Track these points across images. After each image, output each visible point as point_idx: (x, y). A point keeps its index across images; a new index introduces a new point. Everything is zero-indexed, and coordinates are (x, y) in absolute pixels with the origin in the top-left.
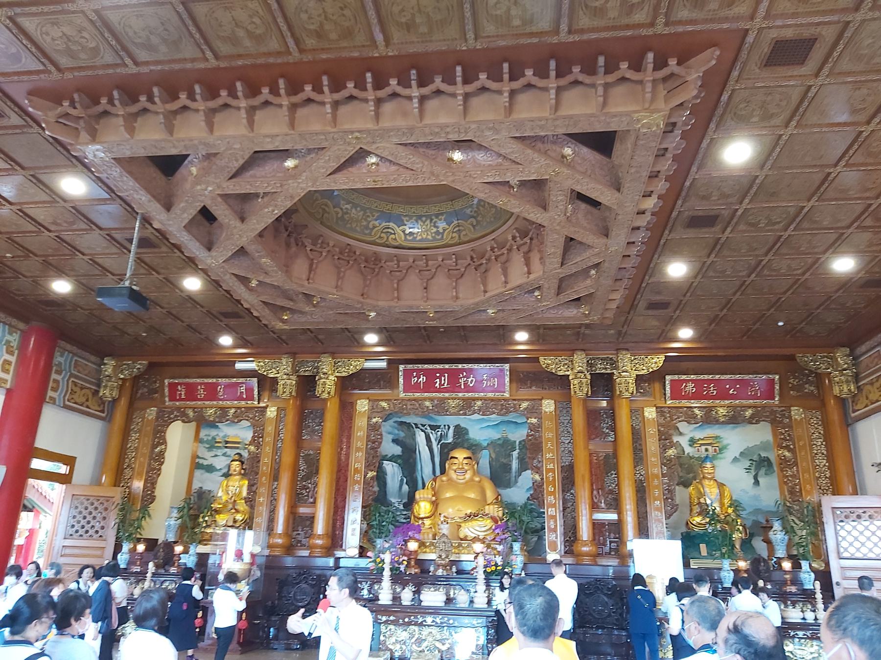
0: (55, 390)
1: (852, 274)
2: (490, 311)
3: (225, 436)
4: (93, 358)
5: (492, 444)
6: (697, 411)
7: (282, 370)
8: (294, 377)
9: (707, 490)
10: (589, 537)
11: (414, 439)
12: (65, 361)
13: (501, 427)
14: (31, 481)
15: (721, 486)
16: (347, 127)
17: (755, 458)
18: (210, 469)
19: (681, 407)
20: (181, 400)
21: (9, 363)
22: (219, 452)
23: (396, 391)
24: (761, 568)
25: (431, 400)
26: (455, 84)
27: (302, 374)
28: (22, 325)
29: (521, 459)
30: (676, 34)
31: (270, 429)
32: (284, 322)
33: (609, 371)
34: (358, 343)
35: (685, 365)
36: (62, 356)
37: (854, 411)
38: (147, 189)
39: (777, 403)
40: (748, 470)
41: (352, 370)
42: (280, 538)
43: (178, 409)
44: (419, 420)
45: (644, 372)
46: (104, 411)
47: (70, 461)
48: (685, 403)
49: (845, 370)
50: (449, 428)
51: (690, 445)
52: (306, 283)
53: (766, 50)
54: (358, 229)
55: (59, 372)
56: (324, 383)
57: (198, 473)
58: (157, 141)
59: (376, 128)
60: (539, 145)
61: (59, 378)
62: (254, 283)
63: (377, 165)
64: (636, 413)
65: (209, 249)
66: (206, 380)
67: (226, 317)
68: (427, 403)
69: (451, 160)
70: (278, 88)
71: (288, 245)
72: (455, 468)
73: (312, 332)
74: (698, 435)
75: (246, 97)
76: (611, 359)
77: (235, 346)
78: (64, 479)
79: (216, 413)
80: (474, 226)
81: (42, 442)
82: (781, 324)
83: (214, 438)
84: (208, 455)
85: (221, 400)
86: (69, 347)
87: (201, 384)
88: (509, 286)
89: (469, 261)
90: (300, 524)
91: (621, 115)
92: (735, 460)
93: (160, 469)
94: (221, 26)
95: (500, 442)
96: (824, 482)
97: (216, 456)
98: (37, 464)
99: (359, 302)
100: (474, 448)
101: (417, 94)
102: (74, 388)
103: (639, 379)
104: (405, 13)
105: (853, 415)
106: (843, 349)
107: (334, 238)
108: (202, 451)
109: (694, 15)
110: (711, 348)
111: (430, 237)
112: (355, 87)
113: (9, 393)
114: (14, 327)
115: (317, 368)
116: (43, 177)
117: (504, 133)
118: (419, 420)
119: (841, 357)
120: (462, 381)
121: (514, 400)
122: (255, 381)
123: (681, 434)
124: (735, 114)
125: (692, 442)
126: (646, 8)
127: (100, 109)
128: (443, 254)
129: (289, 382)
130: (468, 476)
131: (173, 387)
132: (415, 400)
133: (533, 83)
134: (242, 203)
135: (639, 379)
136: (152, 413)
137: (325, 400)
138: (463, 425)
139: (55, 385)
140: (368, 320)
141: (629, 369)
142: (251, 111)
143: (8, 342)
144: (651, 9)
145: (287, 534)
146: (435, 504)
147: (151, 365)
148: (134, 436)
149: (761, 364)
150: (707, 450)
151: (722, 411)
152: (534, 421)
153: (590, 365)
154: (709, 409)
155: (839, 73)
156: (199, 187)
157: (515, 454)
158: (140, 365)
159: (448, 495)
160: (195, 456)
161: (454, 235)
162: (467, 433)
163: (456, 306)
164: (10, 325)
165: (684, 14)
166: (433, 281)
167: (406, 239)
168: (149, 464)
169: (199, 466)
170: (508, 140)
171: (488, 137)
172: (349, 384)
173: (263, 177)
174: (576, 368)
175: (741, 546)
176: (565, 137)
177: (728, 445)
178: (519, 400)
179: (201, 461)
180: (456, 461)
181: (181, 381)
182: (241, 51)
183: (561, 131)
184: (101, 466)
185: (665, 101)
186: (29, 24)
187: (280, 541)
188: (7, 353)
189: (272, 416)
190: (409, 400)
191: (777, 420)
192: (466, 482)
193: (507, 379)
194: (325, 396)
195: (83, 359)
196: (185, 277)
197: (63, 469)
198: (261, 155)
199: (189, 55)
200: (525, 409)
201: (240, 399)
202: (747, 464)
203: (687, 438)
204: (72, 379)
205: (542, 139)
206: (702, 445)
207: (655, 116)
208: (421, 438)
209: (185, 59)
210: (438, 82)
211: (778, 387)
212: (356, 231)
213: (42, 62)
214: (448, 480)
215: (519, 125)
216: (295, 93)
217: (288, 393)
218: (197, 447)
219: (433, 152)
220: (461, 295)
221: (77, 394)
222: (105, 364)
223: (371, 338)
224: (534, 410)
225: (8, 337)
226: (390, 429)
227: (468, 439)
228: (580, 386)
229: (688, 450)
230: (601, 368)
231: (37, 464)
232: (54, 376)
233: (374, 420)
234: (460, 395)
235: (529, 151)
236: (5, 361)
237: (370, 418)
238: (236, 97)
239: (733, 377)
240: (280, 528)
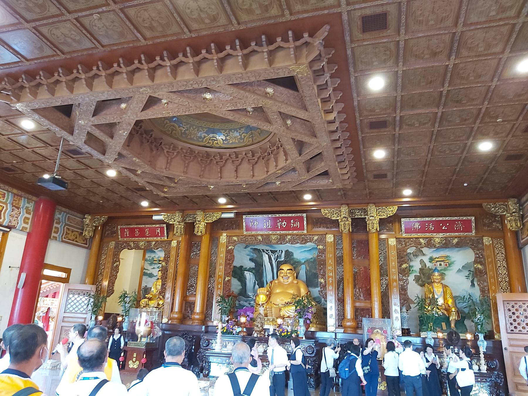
0: (56, 232)
1: (494, 152)
2: (278, 183)
3: (159, 257)
4: (79, 215)
5: (307, 261)
6: (421, 240)
7: (342, 214)
8: (183, 224)
9: (436, 289)
11: (262, 259)
12: (62, 217)
13: (312, 251)
14: (43, 281)
15: (445, 286)
16: (138, 84)
17: (472, 269)
18: (151, 275)
19: (412, 238)
20: (127, 237)
21: (28, 219)
22: (156, 266)
23: (242, 230)
24: (453, 338)
25: (262, 235)
26: (289, 41)
27: (188, 221)
28: (34, 198)
30: (299, 19)
31: (173, 253)
32: (164, 192)
33: (363, 217)
34: (299, 200)
35: (414, 212)
36: (60, 214)
37: (522, 239)
38: (56, 124)
39: (474, 234)
40: (467, 277)
41: (214, 219)
42: (177, 314)
43: (126, 242)
44: (265, 248)
45: (385, 217)
46: (87, 244)
47: (68, 271)
48: (414, 235)
49: (513, 213)
50: (282, 252)
51: (430, 262)
52: (164, 171)
53: (359, 23)
54: (195, 138)
55: (58, 223)
56: (199, 227)
57: (144, 278)
58: (47, 99)
59: (153, 84)
60: (249, 87)
61: (58, 226)
62: (139, 172)
63: (168, 103)
64: (383, 243)
65: (104, 154)
66: (139, 226)
67: (139, 191)
68: (260, 238)
69: (205, 99)
70: (211, 49)
71: (152, 150)
72: (282, 275)
73: (188, 198)
74: (435, 255)
75: (193, 56)
76: (364, 209)
77: (227, 204)
78: (65, 281)
79: (145, 244)
80: (259, 134)
81: (48, 260)
82: (465, 185)
83: (153, 258)
84: (150, 268)
85: (147, 237)
86: (64, 209)
87: (137, 228)
88: (278, 168)
89: (260, 154)
90: (187, 305)
91: (282, 68)
92: (459, 271)
93: (116, 276)
94: (58, 37)
95: (312, 260)
96: (504, 285)
97: (154, 268)
98: (47, 272)
99: (198, 180)
100: (295, 265)
101: (169, 64)
102: (68, 231)
103: (382, 222)
104: (145, 22)
105: (522, 241)
106: (513, 199)
107: (180, 144)
108: (147, 266)
109: (305, 8)
110: (425, 201)
111: (237, 141)
112: (231, 49)
113: (29, 235)
114: (30, 199)
115: (195, 218)
116: (11, 120)
117: (222, 83)
118: (265, 248)
119: (512, 205)
120: (279, 224)
121: (310, 235)
122: (165, 225)
123: (424, 255)
124: (361, 61)
125: (431, 260)
126: (275, 6)
127: (133, 67)
128: (245, 151)
129: (179, 226)
130: (290, 280)
131: (122, 230)
132: (252, 236)
133: (230, 53)
134: (110, 128)
135: (382, 222)
136: (112, 244)
137: (201, 237)
138: (290, 250)
139: (56, 230)
140: (210, 190)
141: (374, 216)
142: (271, 53)
143: (27, 208)
144: (278, 6)
145: (181, 311)
146: (269, 297)
147: (109, 218)
148: (103, 257)
149: (447, 210)
150: (440, 265)
151: (437, 240)
152: (321, 247)
153: (351, 213)
155: (471, 24)
156: (84, 122)
158: (104, 218)
159: (278, 291)
160: (143, 269)
161: (250, 139)
162: (293, 255)
163: (253, 180)
164: (28, 198)
165: (298, 7)
166: (240, 167)
167: (223, 143)
168: (111, 273)
169: (145, 274)
170: (227, 86)
171: (213, 85)
172: (215, 228)
173: (110, 114)
174: (342, 214)
175: (455, 325)
176: (265, 82)
177: (454, 261)
178: (313, 235)
179: (146, 271)
180: (283, 271)
181: (137, 226)
182: (74, 49)
183: (262, 78)
184: (86, 273)
185: (306, 59)
186: (45, 30)
187: (176, 316)
188: (26, 213)
189: (174, 246)
190: (249, 236)
191: (476, 245)
192: (289, 284)
193: (305, 223)
194: (200, 234)
195: (73, 215)
197: (63, 275)
198: (108, 102)
199: (223, 25)
200: (316, 240)
201: (157, 236)
202: (467, 273)
203: (428, 257)
204: (66, 227)
205: (251, 84)
206: (437, 261)
207: (302, 67)
208: (266, 258)
209: (49, 56)
210: (181, 57)
211: (474, 225)
212: (194, 140)
213: (54, 50)
215: (229, 77)
216: (246, 48)
217: (179, 232)
218: (144, 263)
219: (194, 95)
220: (256, 174)
221: (70, 235)
222: (85, 218)
223: (222, 200)
224: (322, 240)
225: (27, 205)
226: (248, 253)
227: (293, 259)
228: (346, 226)
229: (429, 265)
230: (358, 215)
231: (47, 272)
232: (55, 225)
233: (230, 247)
234: (278, 232)
235: (242, 92)
236: (25, 217)
237: (227, 247)
238: (235, 49)
239: (444, 219)
240: (176, 308)
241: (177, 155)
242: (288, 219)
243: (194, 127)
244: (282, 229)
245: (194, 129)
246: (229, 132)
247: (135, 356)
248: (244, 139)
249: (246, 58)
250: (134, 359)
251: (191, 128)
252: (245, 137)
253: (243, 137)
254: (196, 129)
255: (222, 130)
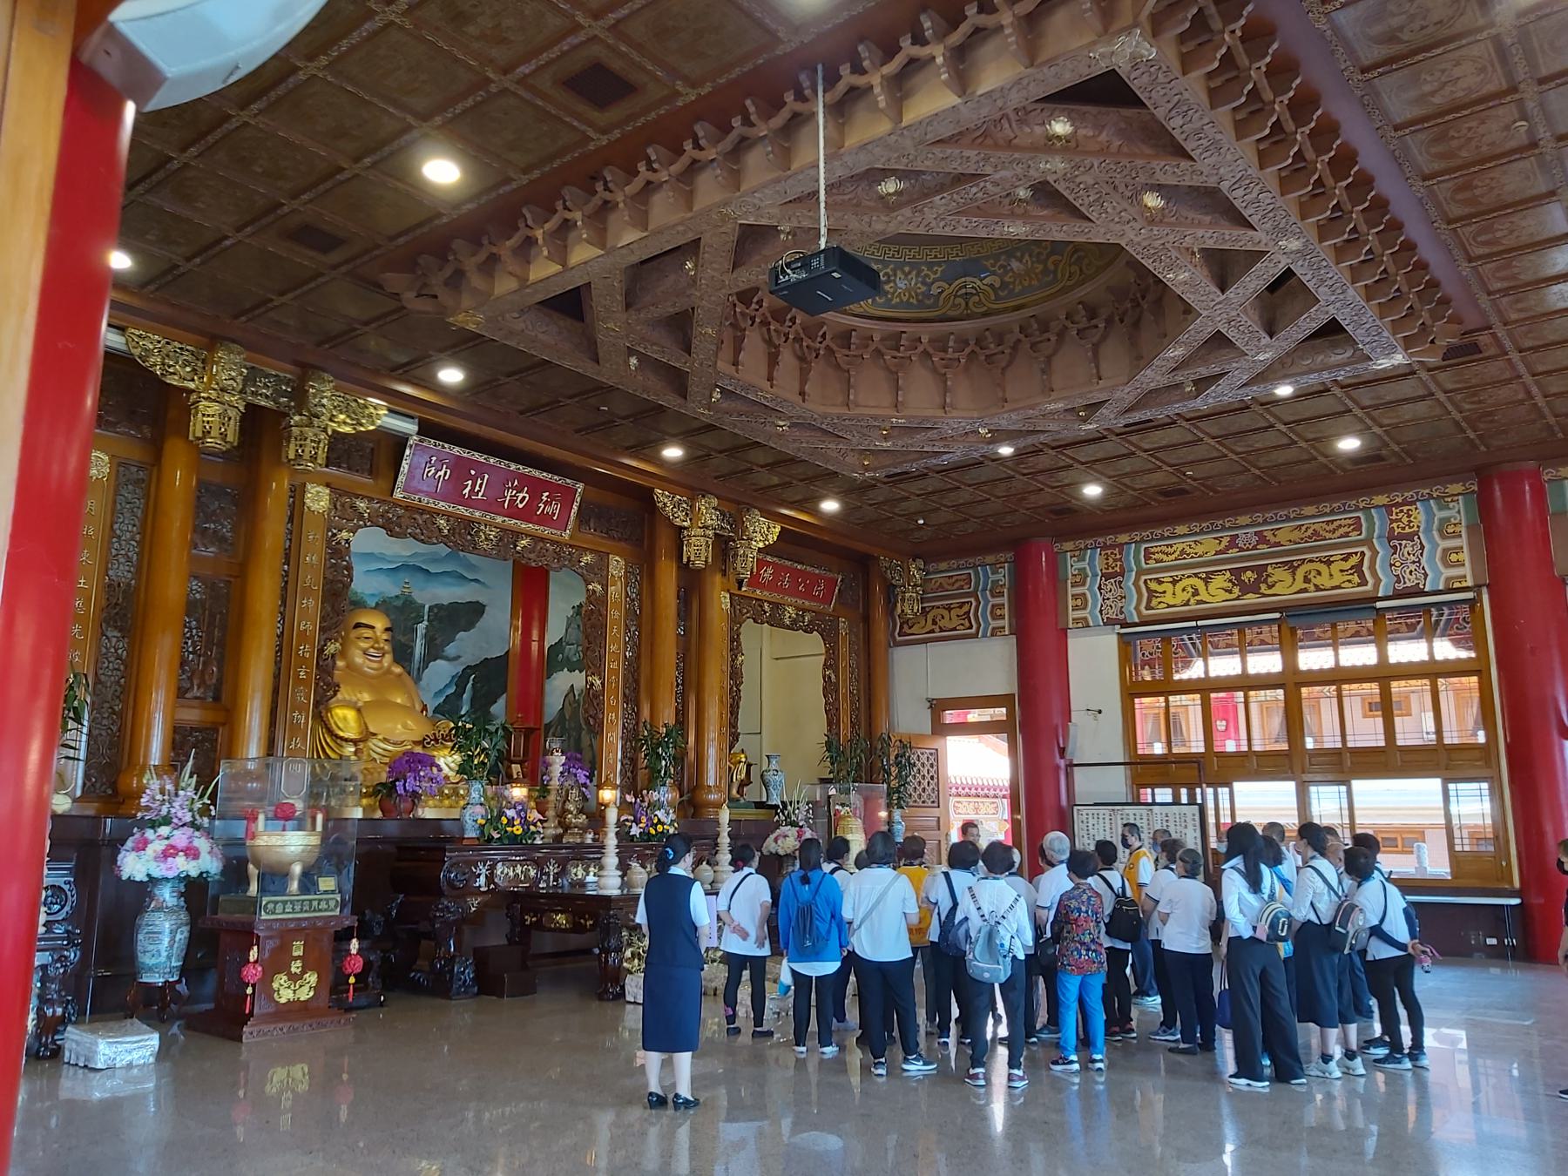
10: (163, 758)
29: (430, 640)
72: (364, 645)
95: (399, 603)
154: (776, 606)
157: (421, 628)
167: (998, 298)
176: (1040, 106)
180: (367, 633)
196: (446, 190)
214: (348, 666)
220: (1103, 373)
224: (598, 571)
234: (499, 519)
241: (1012, 357)
242: (536, 488)
243: (907, 269)
244: (513, 512)
245: (906, 275)
246: (894, 271)
247: (298, 952)
248: (1055, 272)
249: (961, 56)
250: (296, 967)
251: (899, 274)
252: (1056, 264)
253: (1052, 267)
254: (1027, 257)
255: (987, 258)
